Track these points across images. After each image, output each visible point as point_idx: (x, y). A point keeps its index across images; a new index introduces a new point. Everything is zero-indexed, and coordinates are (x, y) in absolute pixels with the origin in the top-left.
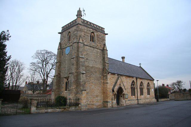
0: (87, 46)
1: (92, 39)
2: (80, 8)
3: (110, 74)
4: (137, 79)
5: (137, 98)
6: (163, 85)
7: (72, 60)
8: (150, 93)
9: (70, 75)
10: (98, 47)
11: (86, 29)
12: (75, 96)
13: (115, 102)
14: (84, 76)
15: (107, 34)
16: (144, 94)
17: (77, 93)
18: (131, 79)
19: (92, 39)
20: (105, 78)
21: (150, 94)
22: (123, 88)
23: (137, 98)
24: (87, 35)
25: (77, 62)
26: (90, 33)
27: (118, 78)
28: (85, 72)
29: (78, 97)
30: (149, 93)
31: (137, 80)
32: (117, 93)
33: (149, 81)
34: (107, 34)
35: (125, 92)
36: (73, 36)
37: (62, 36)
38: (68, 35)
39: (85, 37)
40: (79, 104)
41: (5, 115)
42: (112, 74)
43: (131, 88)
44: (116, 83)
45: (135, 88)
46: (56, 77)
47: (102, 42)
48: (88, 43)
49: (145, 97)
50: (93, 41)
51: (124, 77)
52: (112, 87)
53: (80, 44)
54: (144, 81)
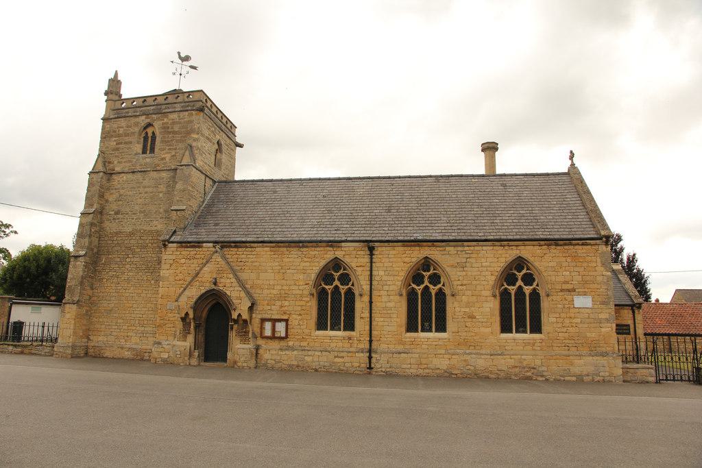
5: (371, 341)
23: (371, 341)
31: (371, 255)
51: (257, 249)
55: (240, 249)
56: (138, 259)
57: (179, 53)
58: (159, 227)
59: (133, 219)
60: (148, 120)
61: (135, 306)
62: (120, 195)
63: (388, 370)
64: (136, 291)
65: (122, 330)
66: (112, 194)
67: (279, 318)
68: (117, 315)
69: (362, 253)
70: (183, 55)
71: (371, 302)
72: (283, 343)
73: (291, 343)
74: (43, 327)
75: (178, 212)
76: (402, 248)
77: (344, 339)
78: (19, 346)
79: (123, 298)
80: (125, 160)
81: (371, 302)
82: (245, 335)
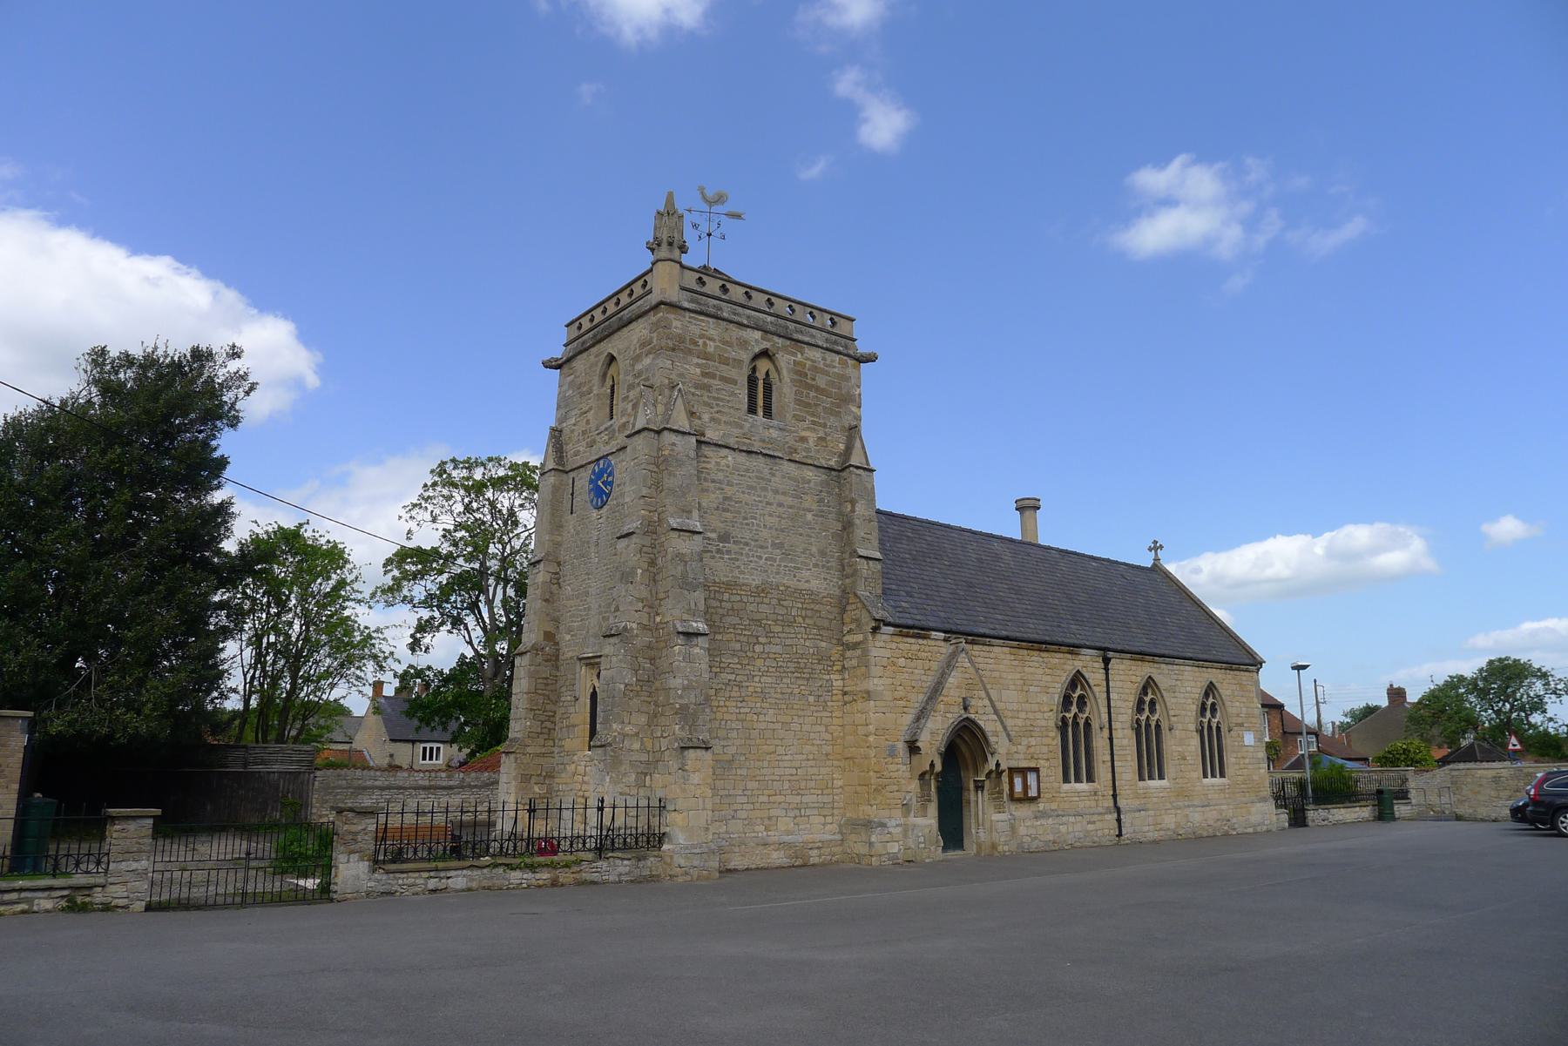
0: (725, 452)
1: (760, 396)
2: (670, 195)
3: (891, 629)
4: (1106, 661)
5: (1115, 796)
6: (1396, 694)
7: (623, 543)
8: (1230, 759)
9: (608, 650)
10: (808, 450)
12: (640, 784)
13: (928, 821)
14: (697, 650)
15: (871, 359)
16: (1169, 769)
17: (646, 770)
18: (1055, 659)
19: (760, 402)
20: (854, 662)
21: (1229, 771)
22: (988, 723)
23: (1115, 796)
24: (723, 379)
25: (652, 563)
26: (746, 357)
27: (950, 664)
28: (701, 626)
29: (660, 794)
30: (1214, 759)
31: (1106, 669)
32: (944, 764)
33: (1215, 675)
34: (871, 359)
35: (1004, 752)
36: (631, 387)
37: (571, 384)
38: (604, 376)
39: (707, 388)
40: (662, 838)
41: (210, 902)
42: (901, 635)
43: (1063, 726)
44: (936, 691)
45: (1095, 725)
47: (838, 414)
48: (736, 431)
50: (768, 412)
51: (996, 649)
52: (908, 719)
53: (672, 438)
54: (1163, 674)
55: (976, 647)
56: (778, 649)
57: (702, 190)
58: (815, 584)
59: (760, 558)
60: (766, 345)
61: (780, 750)
62: (726, 498)
63: (1133, 835)
64: (781, 718)
65: (757, 805)
66: (707, 491)
67: (1026, 766)
68: (744, 772)
69: (1096, 665)
70: (710, 194)
71: (1111, 739)
72: (1033, 807)
73: (1041, 806)
74: (601, 809)
75: (871, 562)
76: (1128, 662)
77: (1091, 795)
78: (541, 865)
79: (755, 733)
80: (724, 419)
81: (1111, 739)
82: (998, 798)
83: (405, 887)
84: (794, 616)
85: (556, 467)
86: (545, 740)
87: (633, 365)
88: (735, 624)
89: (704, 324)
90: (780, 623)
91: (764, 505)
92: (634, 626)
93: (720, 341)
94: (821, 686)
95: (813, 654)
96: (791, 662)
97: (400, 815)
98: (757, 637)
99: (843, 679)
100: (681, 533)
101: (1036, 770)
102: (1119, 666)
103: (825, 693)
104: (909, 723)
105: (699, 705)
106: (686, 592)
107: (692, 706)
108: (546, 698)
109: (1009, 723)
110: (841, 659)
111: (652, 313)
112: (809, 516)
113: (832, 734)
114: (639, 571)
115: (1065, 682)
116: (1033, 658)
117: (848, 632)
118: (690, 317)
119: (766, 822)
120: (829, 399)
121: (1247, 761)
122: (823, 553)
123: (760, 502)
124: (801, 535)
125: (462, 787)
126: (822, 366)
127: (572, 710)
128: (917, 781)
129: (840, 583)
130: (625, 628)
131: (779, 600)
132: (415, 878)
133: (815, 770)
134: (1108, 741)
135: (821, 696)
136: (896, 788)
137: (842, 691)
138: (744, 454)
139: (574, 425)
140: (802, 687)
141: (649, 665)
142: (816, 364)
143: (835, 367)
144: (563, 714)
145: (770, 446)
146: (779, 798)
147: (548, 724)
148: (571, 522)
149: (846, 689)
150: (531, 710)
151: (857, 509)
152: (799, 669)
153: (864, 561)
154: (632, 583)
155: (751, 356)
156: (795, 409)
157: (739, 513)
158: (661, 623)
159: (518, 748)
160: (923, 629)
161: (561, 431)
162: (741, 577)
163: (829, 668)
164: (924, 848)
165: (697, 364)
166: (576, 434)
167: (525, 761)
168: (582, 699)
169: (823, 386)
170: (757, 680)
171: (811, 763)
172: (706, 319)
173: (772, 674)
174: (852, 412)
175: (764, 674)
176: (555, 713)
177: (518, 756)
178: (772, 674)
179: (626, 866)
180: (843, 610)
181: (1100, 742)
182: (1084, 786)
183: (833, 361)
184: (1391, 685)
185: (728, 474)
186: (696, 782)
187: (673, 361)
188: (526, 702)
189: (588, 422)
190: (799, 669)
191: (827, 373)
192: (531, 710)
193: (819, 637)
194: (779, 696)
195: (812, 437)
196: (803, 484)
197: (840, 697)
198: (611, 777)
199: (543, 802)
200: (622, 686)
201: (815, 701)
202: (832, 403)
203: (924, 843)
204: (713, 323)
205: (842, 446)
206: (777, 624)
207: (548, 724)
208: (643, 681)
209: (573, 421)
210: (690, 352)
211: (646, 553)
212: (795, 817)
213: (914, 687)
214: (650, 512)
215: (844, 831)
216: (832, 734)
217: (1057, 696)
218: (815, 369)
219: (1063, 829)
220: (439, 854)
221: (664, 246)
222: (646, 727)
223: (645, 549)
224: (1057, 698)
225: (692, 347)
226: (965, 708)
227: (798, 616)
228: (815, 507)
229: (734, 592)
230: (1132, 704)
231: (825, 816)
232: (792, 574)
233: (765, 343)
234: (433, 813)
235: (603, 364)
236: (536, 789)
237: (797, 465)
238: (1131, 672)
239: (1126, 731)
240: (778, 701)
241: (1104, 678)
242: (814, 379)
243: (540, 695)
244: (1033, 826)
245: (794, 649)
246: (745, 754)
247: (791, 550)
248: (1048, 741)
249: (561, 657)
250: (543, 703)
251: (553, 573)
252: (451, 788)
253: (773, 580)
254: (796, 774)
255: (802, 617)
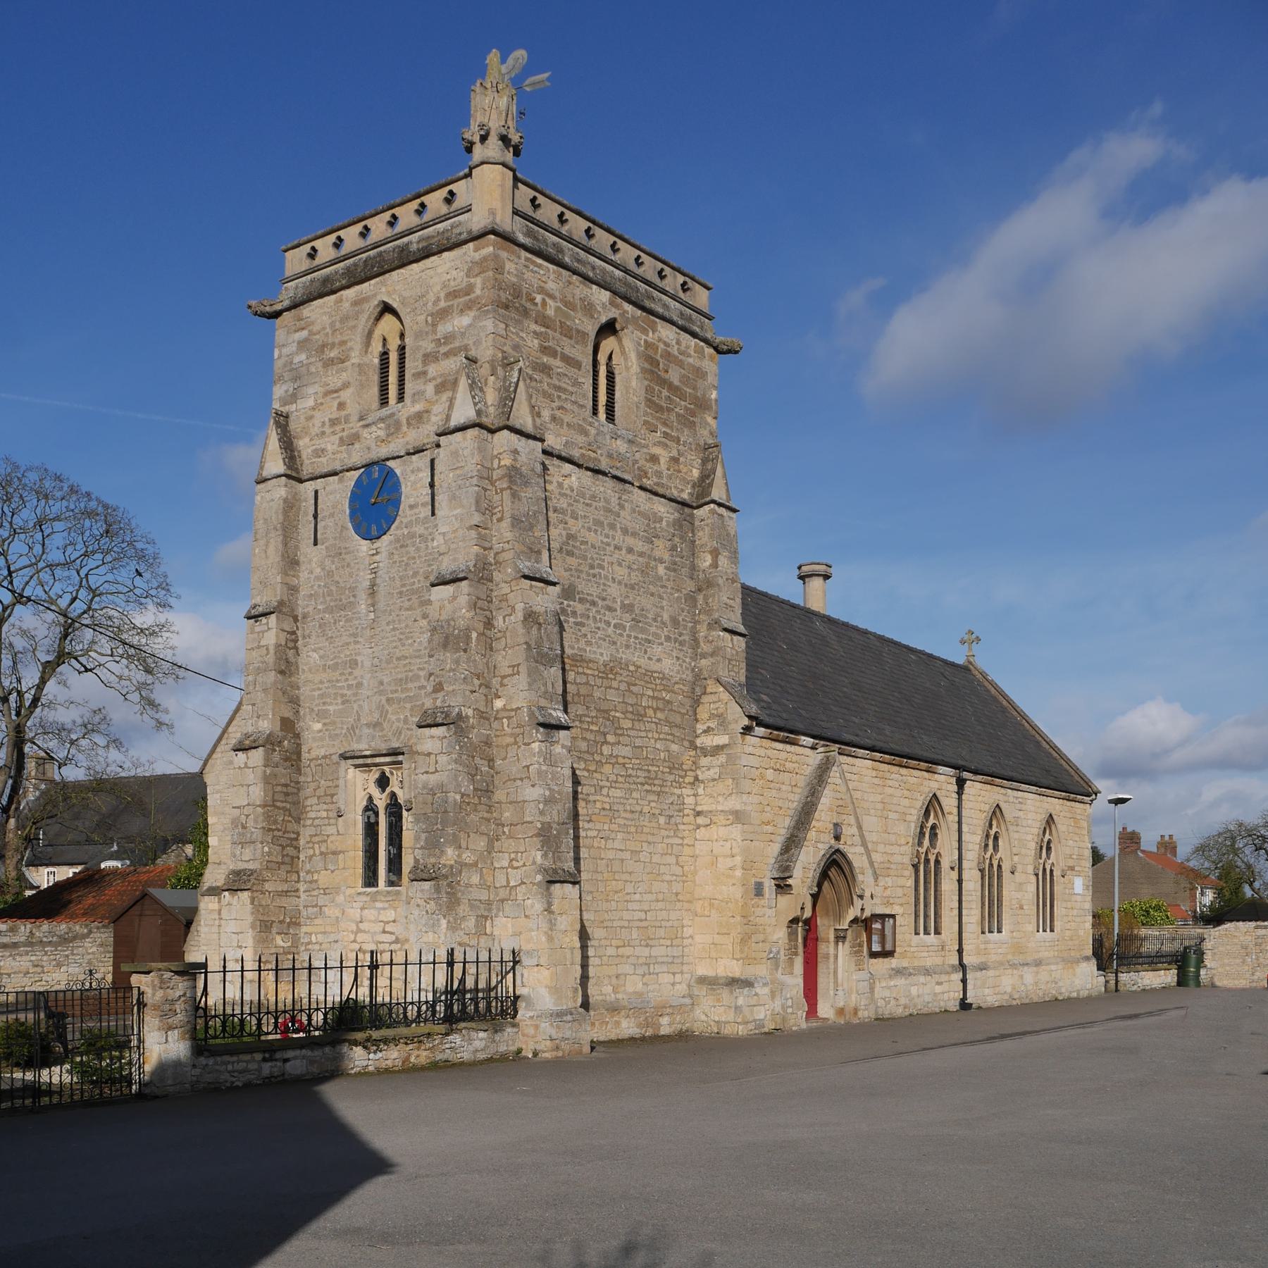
4: (961, 783)
5: (960, 951)
10: (659, 474)
11: (551, 286)
23: (960, 951)
26: (591, 329)
29: (508, 946)
31: (960, 792)
36: (429, 358)
39: (546, 369)
45: (945, 864)
46: (257, 756)
48: (581, 439)
49: (1018, 949)
56: (626, 751)
61: (629, 888)
71: (960, 881)
74: (451, 964)
81: (960, 881)
83: (236, 1074)
84: (645, 707)
85: (289, 472)
86: (287, 872)
87: (434, 325)
88: (581, 716)
89: (542, 272)
90: (629, 716)
91: (612, 548)
92: (470, 712)
93: (561, 300)
94: (672, 803)
95: (664, 760)
96: (641, 769)
97: (423, 961)
98: (605, 735)
99: (695, 795)
100: (534, 583)
101: (893, 916)
102: (974, 788)
103: (676, 813)
104: (776, 855)
105: (563, 824)
106: (542, 668)
107: (555, 826)
108: (287, 813)
109: (875, 856)
110: (694, 768)
111: (471, 245)
112: (661, 570)
113: (682, 867)
114: (474, 635)
115: (921, 808)
116: (893, 776)
117: (705, 732)
118: (527, 259)
119: (614, 981)
120: (683, 403)
121: (1075, 912)
122: (675, 622)
123: (608, 545)
124: (652, 595)
125: (31, 944)
126: (676, 353)
127: (331, 830)
128: (785, 929)
129: (693, 664)
130: (459, 715)
131: (629, 684)
132: (247, 1062)
133: (664, 914)
134: (957, 883)
135: (672, 816)
136: (761, 937)
137: (694, 810)
138: (589, 473)
139: (314, 409)
140: (653, 804)
141: (487, 768)
142: (668, 349)
143: (689, 356)
144: (311, 836)
145: (619, 465)
146: (627, 951)
147: (290, 851)
148: (311, 557)
149: (699, 808)
150: (270, 830)
151: (719, 563)
152: (649, 780)
153: (727, 635)
154: (465, 651)
155: (597, 327)
156: (646, 414)
157: (585, 558)
158: (504, 709)
159: (254, 884)
160: (791, 732)
161: (287, 417)
162: (588, 649)
163: (681, 780)
164: (793, 1013)
165: (535, 332)
166: (317, 422)
167: (264, 903)
168: (349, 816)
169: (676, 383)
170: (605, 794)
171: (660, 905)
172: (546, 264)
173: (621, 785)
174: (708, 424)
175: (613, 785)
176: (298, 834)
177: (255, 894)
178: (621, 785)
179: (481, 1040)
180: (697, 702)
181: (948, 885)
182: (932, 938)
183: (688, 347)
184: (1124, 829)
185: (571, 501)
186: (563, 927)
187: (507, 326)
188: (261, 818)
189: (341, 406)
190: (649, 780)
191: (681, 364)
192: (270, 830)
193: (668, 737)
194: (628, 815)
195: (664, 455)
196: (654, 522)
197: (692, 818)
198: (449, 922)
199: (288, 959)
200: (458, 797)
201: (665, 823)
202: (686, 409)
203: (792, 1007)
204: (554, 272)
205: (696, 473)
206: (626, 718)
207: (290, 851)
208: (481, 791)
209: (311, 402)
210: (526, 313)
211: (481, 609)
212: (644, 976)
213: (781, 808)
214: (485, 549)
215: (696, 993)
216: (682, 867)
217: (913, 825)
218: (667, 355)
219: (914, 990)
220: (218, 1033)
221: (493, 140)
222: (485, 853)
223: (480, 603)
224: (913, 828)
225: (528, 305)
226: (837, 838)
227: (649, 707)
228: (666, 557)
229: (580, 670)
230: (980, 837)
231: (674, 974)
232: (643, 648)
233: (613, 310)
234: (434, 963)
235: (369, 318)
236: (279, 941)
237: (649, 495)
238: (980, 798)
239: (973, 871)
240: (627, 823)
241: (956, 804)
242: (667, 371)
243: (278, 808)
244: (889, 988)
245: (645, 753)
246: (591, 892)
247: (642, 615)
248: (901, 881)
249: (305, 756)
250: (283, 820)
251: (288, 632)
252: (15, 945)
253: (624, 655)
254: (646, 920)
255: (652, 708)
